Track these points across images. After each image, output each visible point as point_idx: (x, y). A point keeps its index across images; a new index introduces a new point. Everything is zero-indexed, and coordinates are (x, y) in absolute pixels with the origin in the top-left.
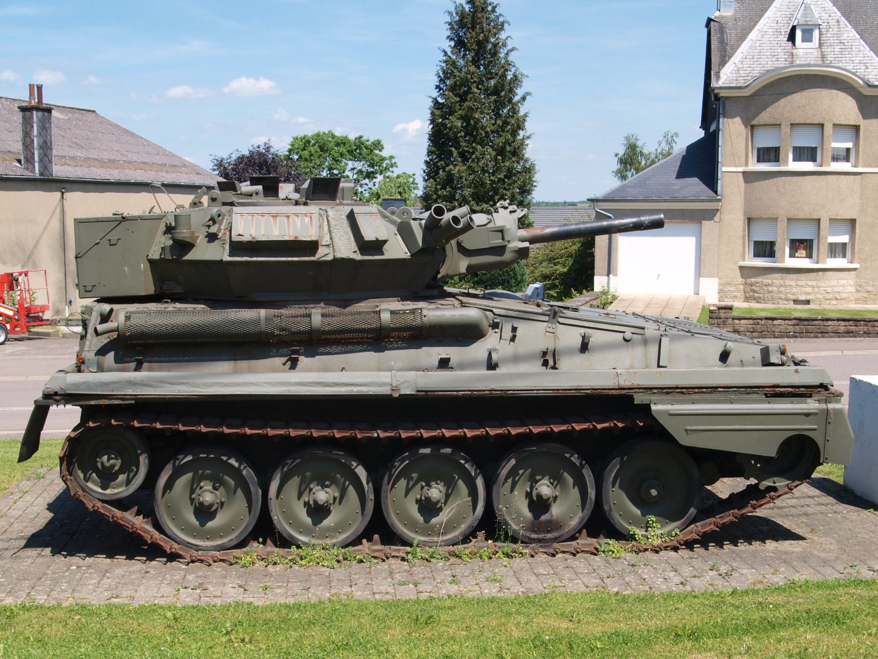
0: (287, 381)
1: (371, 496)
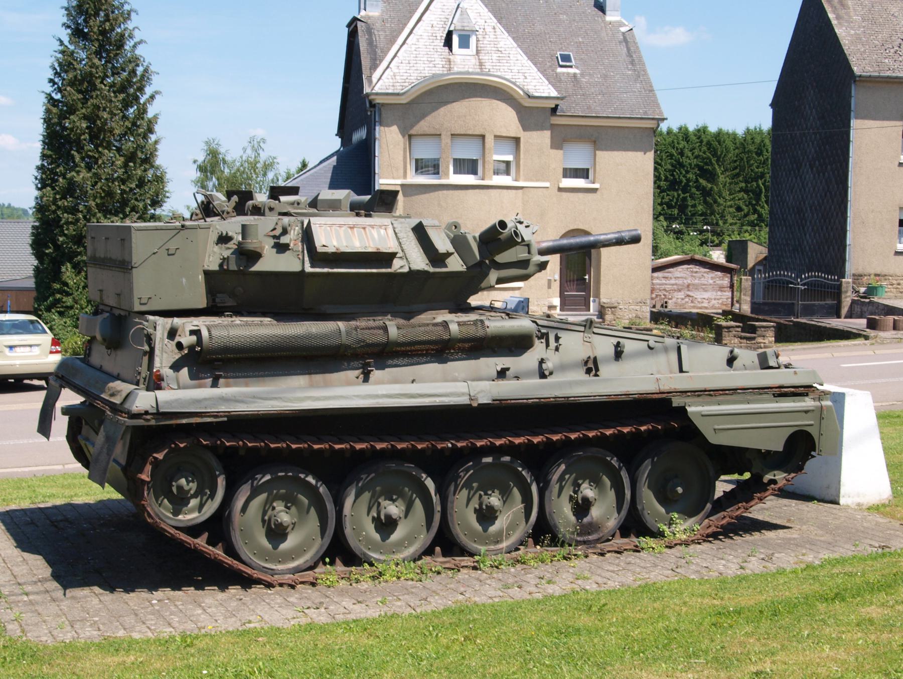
0: (375, 393)
1: (438, 508)
